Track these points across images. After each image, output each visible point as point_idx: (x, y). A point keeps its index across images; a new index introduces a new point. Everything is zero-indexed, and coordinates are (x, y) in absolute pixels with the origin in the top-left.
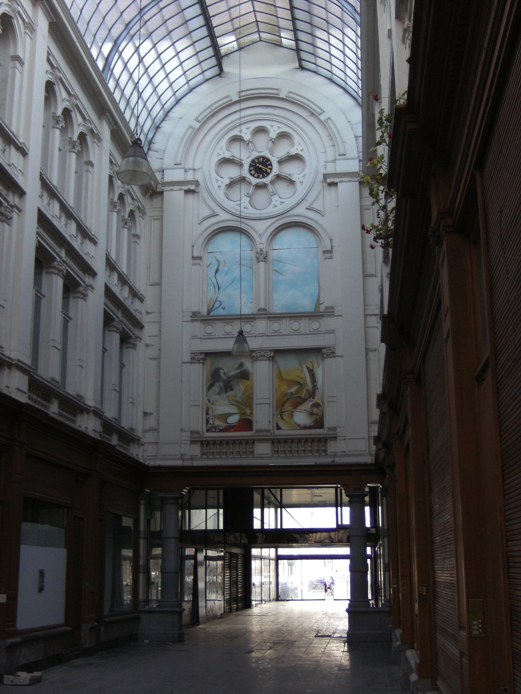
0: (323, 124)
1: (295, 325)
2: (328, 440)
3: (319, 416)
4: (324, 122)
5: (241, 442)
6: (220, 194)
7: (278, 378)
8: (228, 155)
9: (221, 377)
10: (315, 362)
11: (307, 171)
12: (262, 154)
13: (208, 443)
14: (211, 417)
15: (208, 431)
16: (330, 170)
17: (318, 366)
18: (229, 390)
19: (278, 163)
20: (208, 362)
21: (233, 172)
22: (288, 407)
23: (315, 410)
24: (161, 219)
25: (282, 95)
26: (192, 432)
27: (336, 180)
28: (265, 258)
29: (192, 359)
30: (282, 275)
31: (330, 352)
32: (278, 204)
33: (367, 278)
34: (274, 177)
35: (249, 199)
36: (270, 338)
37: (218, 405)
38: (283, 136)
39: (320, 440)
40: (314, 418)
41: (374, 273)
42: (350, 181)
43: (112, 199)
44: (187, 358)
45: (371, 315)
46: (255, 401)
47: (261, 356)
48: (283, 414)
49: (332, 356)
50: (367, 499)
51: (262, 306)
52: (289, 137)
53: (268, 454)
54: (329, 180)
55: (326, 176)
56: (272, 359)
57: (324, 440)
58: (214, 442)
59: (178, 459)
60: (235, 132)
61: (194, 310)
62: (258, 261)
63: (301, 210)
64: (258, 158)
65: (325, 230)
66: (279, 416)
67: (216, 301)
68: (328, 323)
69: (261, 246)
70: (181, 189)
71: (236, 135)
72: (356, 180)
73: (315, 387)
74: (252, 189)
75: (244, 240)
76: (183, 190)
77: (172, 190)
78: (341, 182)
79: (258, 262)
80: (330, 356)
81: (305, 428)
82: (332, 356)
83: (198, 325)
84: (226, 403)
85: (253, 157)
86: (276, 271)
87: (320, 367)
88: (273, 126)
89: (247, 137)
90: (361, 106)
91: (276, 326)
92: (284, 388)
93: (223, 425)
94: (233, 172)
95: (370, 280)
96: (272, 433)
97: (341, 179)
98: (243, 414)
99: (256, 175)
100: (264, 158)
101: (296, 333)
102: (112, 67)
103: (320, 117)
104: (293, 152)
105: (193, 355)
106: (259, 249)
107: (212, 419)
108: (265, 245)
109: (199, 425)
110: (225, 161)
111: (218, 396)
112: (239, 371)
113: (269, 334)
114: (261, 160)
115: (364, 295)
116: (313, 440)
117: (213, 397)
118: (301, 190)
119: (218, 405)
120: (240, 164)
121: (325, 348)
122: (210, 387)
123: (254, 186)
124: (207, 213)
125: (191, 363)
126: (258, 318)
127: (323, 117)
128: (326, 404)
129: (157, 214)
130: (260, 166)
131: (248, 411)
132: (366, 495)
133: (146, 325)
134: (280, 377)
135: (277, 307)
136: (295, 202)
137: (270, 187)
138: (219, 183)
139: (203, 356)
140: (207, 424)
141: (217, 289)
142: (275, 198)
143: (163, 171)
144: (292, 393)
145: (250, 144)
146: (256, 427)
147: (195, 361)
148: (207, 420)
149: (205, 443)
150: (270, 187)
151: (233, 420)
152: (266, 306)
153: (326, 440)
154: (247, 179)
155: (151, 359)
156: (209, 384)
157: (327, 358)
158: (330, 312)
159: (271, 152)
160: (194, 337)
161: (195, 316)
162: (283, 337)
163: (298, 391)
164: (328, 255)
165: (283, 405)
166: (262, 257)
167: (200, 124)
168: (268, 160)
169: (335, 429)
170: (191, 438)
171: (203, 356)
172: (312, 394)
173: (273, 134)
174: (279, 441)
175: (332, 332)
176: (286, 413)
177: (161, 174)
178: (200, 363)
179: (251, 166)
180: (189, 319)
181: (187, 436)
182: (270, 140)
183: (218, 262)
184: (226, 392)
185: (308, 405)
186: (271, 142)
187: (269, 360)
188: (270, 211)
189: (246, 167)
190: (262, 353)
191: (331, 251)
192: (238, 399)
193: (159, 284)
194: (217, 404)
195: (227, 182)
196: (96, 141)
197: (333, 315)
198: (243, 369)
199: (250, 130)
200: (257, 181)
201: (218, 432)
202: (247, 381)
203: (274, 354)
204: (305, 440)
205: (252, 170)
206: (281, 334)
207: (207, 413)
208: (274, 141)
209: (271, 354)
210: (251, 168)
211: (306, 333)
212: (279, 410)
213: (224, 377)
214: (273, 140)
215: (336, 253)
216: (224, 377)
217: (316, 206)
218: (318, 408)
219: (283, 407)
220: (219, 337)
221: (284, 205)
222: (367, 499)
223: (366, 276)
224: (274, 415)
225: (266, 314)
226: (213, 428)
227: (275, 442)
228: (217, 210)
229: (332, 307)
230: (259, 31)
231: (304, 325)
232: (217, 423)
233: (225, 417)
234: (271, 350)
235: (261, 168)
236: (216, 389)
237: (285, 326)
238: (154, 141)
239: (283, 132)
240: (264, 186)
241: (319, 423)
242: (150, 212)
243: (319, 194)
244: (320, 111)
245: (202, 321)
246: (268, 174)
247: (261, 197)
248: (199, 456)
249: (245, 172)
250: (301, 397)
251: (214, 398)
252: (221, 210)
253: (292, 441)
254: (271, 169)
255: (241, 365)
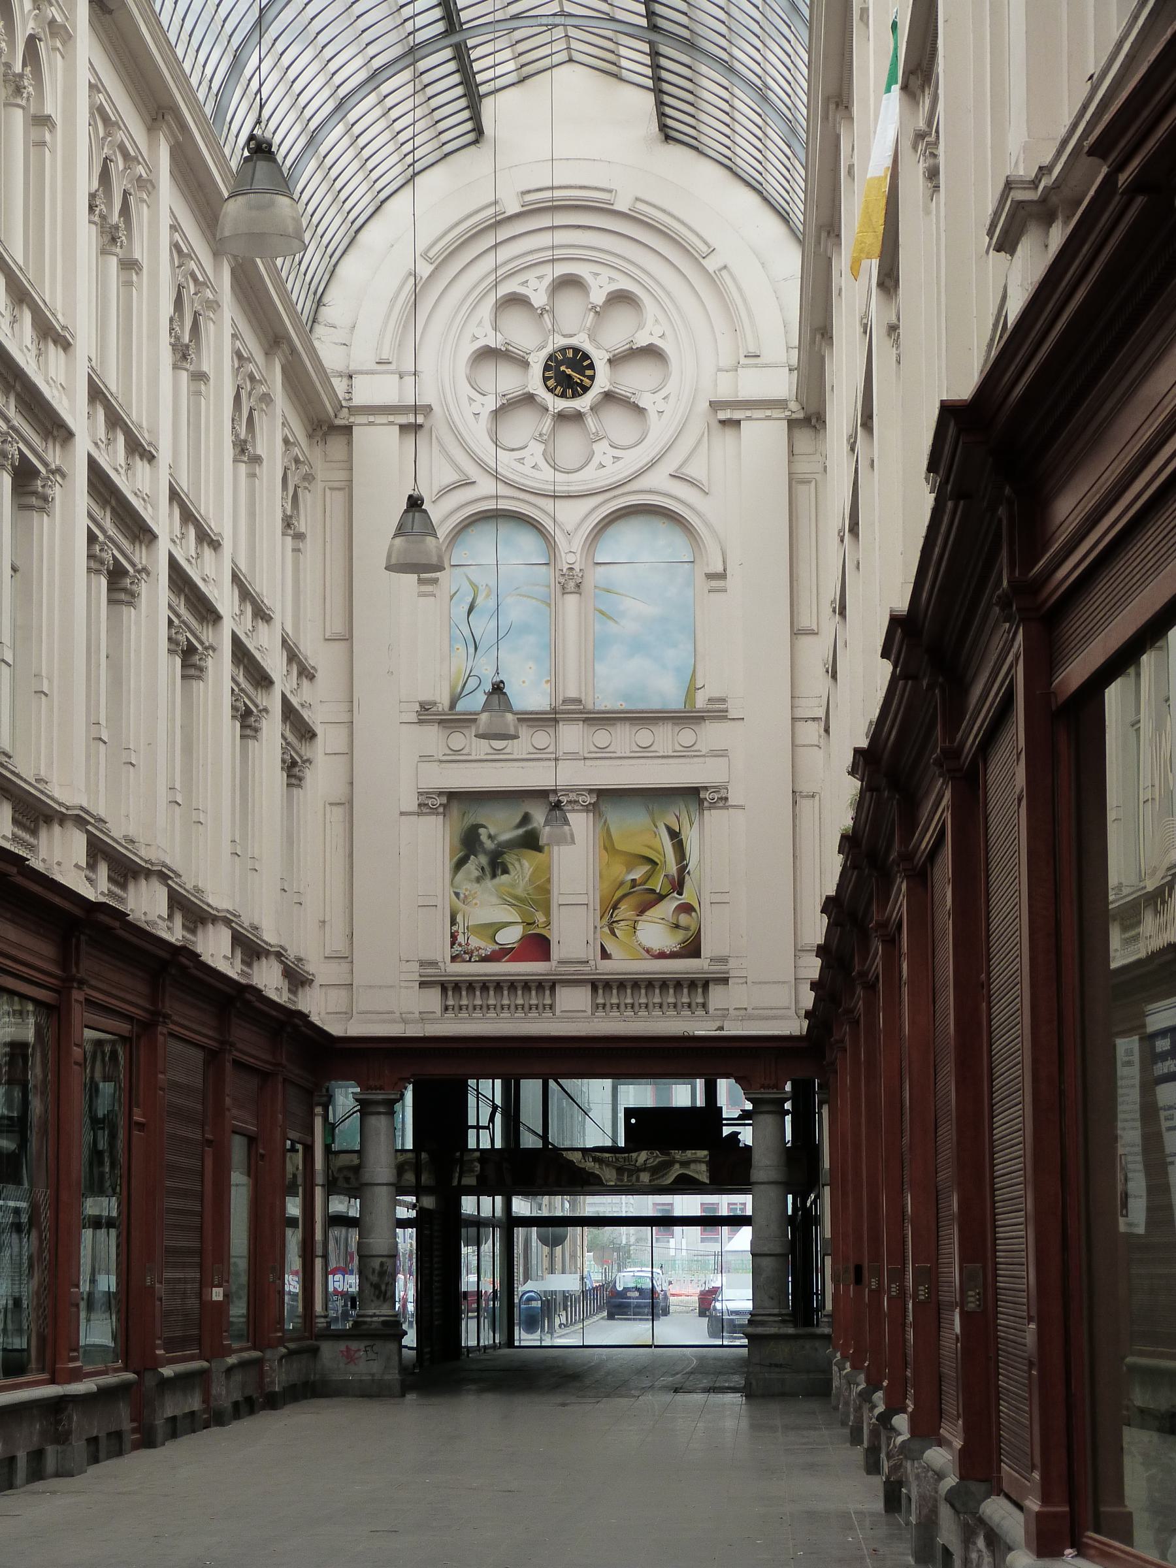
0: (710, 278)
1: (644, 736)
2: (711, 987)
3: (691, 933)
4: (713, 275)
5: (526, 986)
6: (478, 433)
7: (606, 848)
8: (493, 340)
9: (481, 843)
10: (684, 815)
11: (671, 387)
12: (574, 341)
13: (457, 987)
14: (461, 930)
15: (454, 959)
16: (724, 392)
17: (691, 824)
18: (499, 872)
19: (608, 364)
20: (455, 810)
21: (509, 381)
22: (625, 911)
23: (684, 919)
24: (348, 487)
25: (621, 206)
26: (423, 964)
27: (737, 415)
28: (578, 586)
29: (420, 805)
30: (616, 622)
31: (716, 796)
32: (607, 461)
33: (799, 636)
34: (600, 397)
35: (543, 447)
36: (588, 763)
37: (476, 904)
38: (621, 298)
39: (692, 984)
40: (680, 935)
41: (814, 627)
42: (768, 418)
43: (177, 338)
44: (410, 803)
45: (806, 720)
46: (556, 899)
47: (570, 802)
48: (614, 925)
49: (721, 805)
50: (788, 1106)
51: (572, 693)
52: (634, 300)
53: (585, 1011)
54: (722, 415)
55: (715, 406)
56: (593, 808)
57: (701, 985)
58: (471, 986)
59: (394, 1021)
60: (505, 289)
61: (425, 697)
62: (564, 592)
63: (658, 479)
64: (563, 350)
65: (706, 523)
66: (606, 930)
67: (469, 676)
68: (712, 734)
69: (571, 558)
70: (391, 423)
71: (514, 293)
72: (783, 416)
73: (683, 870)
74: (548, 423)
75: (526, 544)
76: (396, 424)
77: (371, 424)
78: (749, 418)
79: (563, 594)
80: (718, 805)
81: (662, 955)
82: (721, 805)
83: (432, 733)
84: (494, 900)
85: (549, 349)
86: (601, 612)
87: (696, 825)
88: (598, 274)
89: (539, 299)
90: (801, 242)
91: (602, 737)
92: (618, 870)
93: (488, 948)
94: (509, 381)
95: (805, 641)
96: (594, 968)
97: (748, 413)
98: (529, 924)
99: (559, 390)
100: (576, 350)
101: (645, 753)
102: (228, 119)
103: (704, 262)
104: (642, 340)
105: (424, 797)
106: (565, 567)
107: (464, 933)
108: (578, 555)
109: (441, 951)
110: (487, 354)
111: (476, 885)
112: (521, 831)
113: (587, 755)
114: (570, 354)
115: (795, 923)
116: (678, 984)
117: (466, 887)
118: (659, 430)
119: (476, 904)
120: (524, 363)
121: (706, 788)
122: (460, 864)
123: (554, 416)
124: (451, 477)
125: (419, 814)
126: (564, 720)
127: (711, 264)
128: (705, 905)
129: (342, 475)
130: (569, 371)
131: (540, 918)
132: (786, 1100)
133: (319, 730)
134: (609, 846)
135: (605, 700)
136: (646, 459)
137: (590, 421)
138: (476, 408)
139: (444, 800)
140: (453, 944)
141: (472, 650)
142: (601, 447)
143: (351, 377)
144: (634, 880)
145: (546, 316)
146: (556, 952)
147: (428, 811)
148: (454, 937)
149: (450, 987)
150: (589, 419)
151: (510, 936)
152: (580, 692)
153: (706, 984)
154: (538, 399)
155: (331, 804)
156: (455, 859)
157: (710, 809)
158: (718, 713)
159: (592, 338)
160: (425, 758)
161: (426, 713)
162: (619, 762)
163: (648, 877)
164: (715, 584)
165: (615, 907)
166: (572, 584)
167: (433, 267)
168: (586, 356)
169: (723, 960)
170: (420, 976)
171: (444, 800)
172: (678, 885)
173: (598, 297)
174: (607, 985)
175: (722, 754)
176: (622, 923)
177: (345, 381)
178: (438, 814)
179: (547, 368)
180: (413, 717)
181: (414, 972)
182: (591, 310)
183: (475, 587)
184: (494, 876)
185: (667, 908)
186: (592, 314)
187: (588, 811)
188: (591, 477)
189: (537, 369)
190: (573, 796)
191: (722, 576)
192: (519, 892)
193: (347, 638)
194: (474, 902)
195: (491, 403)
196: (59, 45)
197: (725, 718)
198: (530, 827)
199: (548, 280)
200: (562, 404)
201: (476, 961)
202: (538, 854)
203: (598, 797)
204: (663, 984)
205: (550, 378)
206: (614, 755)
207: (453, 922)
208: (598, 312)
209: (591, 799)
210: (547, 374)
211: (666, 754)
212: (607, 917)
213: (489, 845)
214: (598, 309)
215: (732, 582)
216: (489, 845)
217: (691, 471)
218: (690, 915)
219: (616, 912)
220: (478, 757)
221: (620, 464)
222: (788, 1106)
223: (797, 632)
224: (595, 927)
225: (581, 713)
226: (465, 953)
227: (598, 985)
228: (473, 472)
229: (723, 700)
230: (568, 48)
231: (663, 738)
232: (475, 942)
233: (495, 928)
234: (591, 791)
235: (569, 376)
236: (472, 867)
237: (622, 738)
238: (325, 300)
239: (621, 290)
240: (578, 417)
241: (692, 949)
242: (322, 472)
243: (699, 442)
244: (704, 249)
245: (441, 722)
246: (586, 389)
247: (570, 443)
248: (439, 1014)
249: (534, 382)
250: (653, 891)
251: (466, 890)
252: (481, 470)
253: (636, 984)
254: (592, 378)
255: (526, 819)
